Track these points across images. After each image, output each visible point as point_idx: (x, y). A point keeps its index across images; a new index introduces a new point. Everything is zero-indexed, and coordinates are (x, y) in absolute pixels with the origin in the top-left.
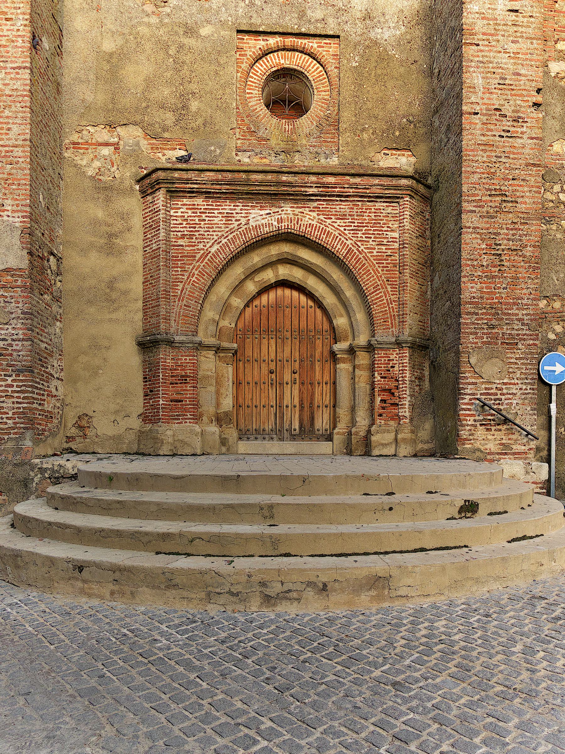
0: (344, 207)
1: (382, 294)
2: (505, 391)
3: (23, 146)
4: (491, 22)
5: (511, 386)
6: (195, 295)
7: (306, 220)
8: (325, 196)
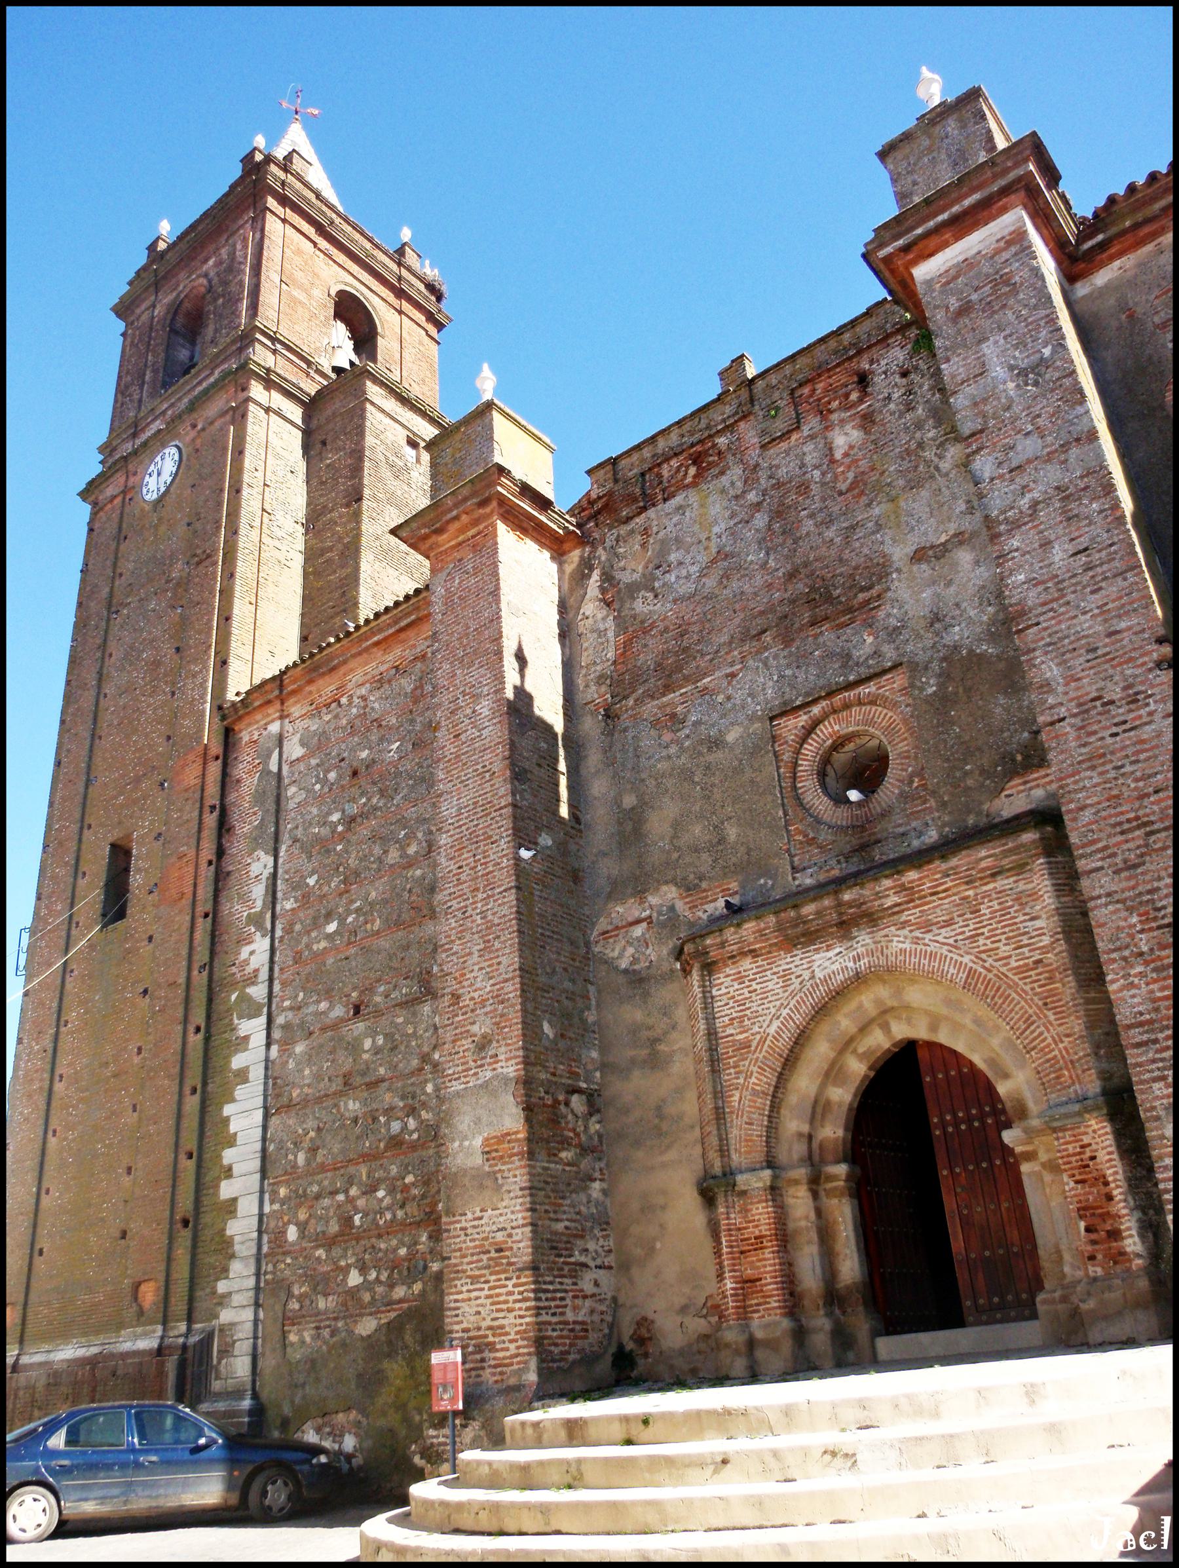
1: (1042, 1029)
3: (513, 979)
4: (1050, 584)
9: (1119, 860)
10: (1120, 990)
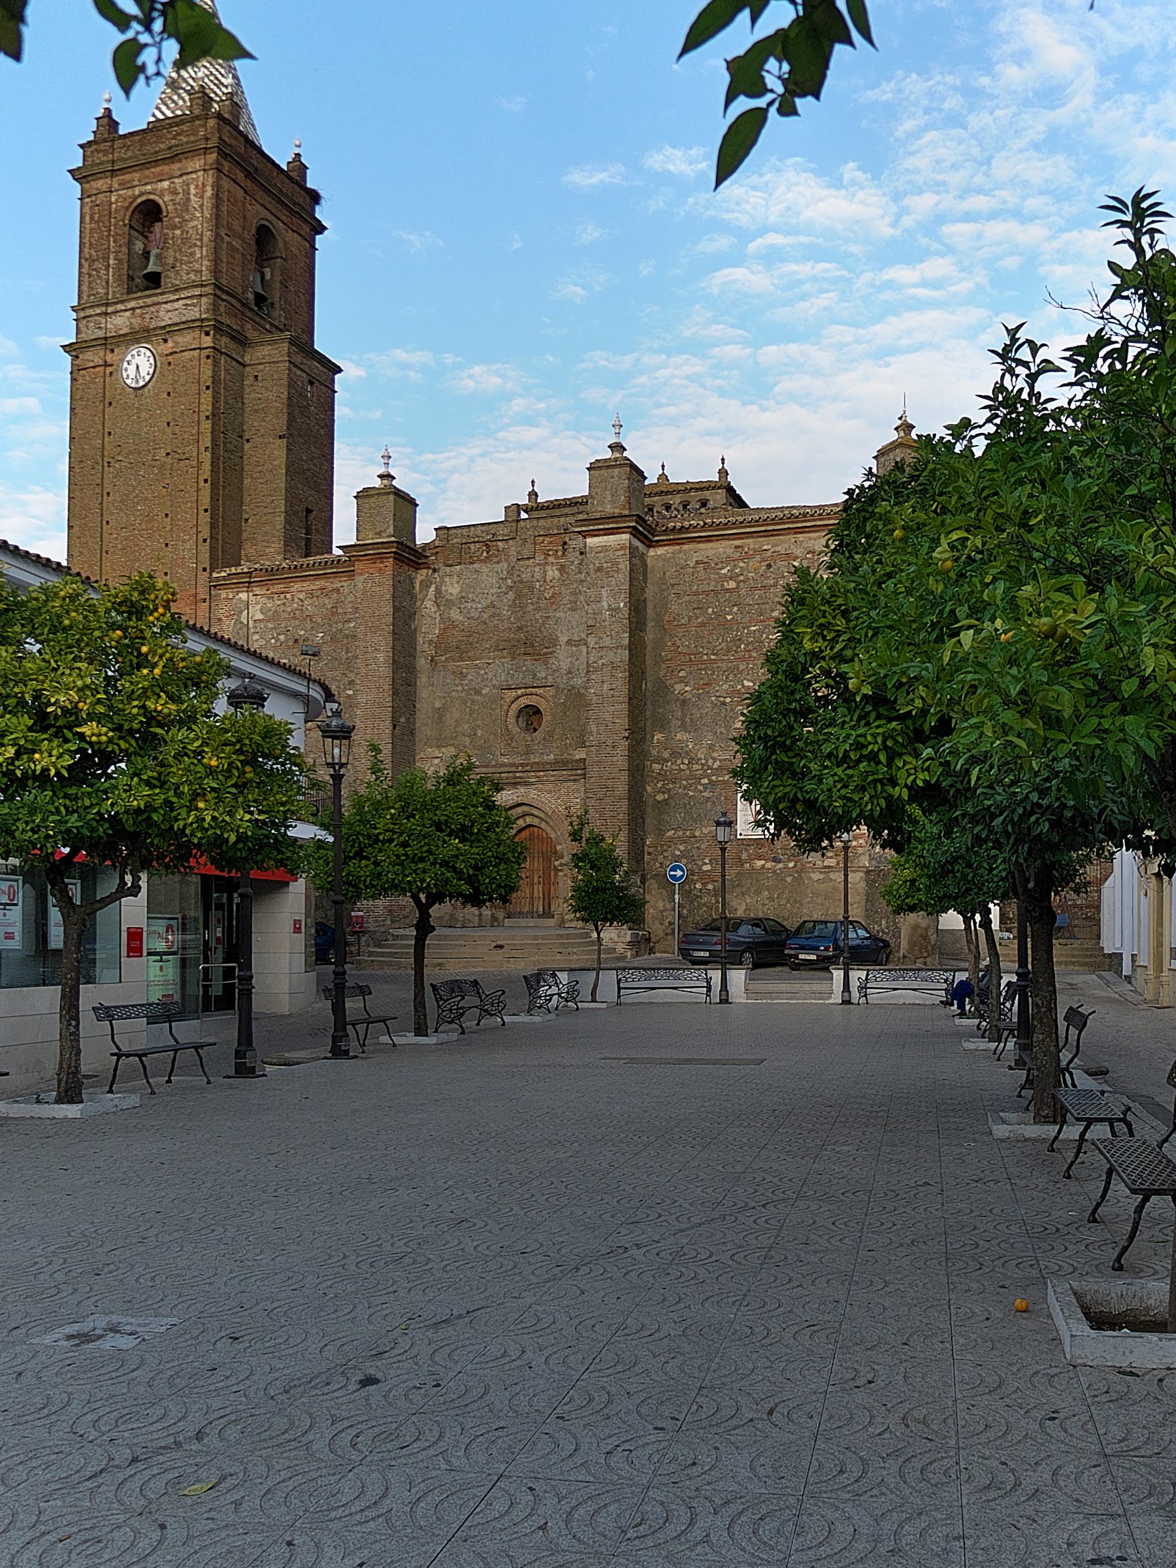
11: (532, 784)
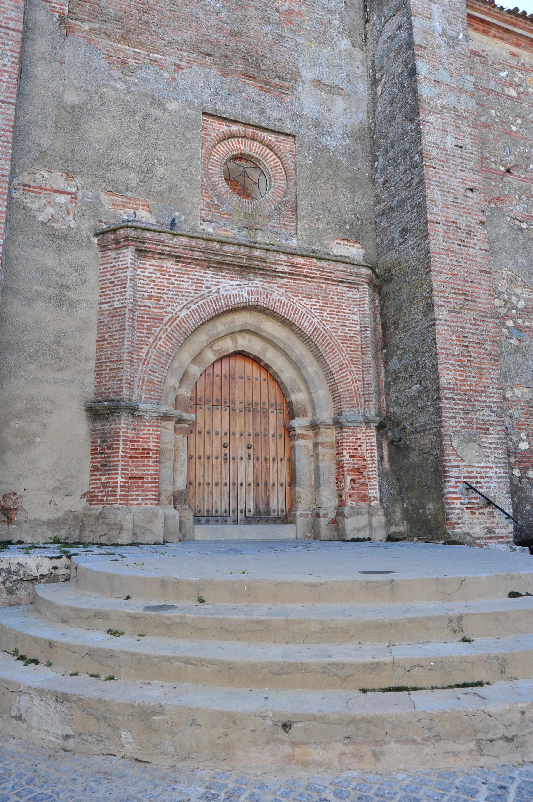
0: (309, 286)
1: (348, 373)
2: (483, 475)
5: (488, 470)
6: (162, 360)
7: (275, 296)
8: (293, 274)
9: (451, 305)
10: (444, 369)
11: (276, 275)
